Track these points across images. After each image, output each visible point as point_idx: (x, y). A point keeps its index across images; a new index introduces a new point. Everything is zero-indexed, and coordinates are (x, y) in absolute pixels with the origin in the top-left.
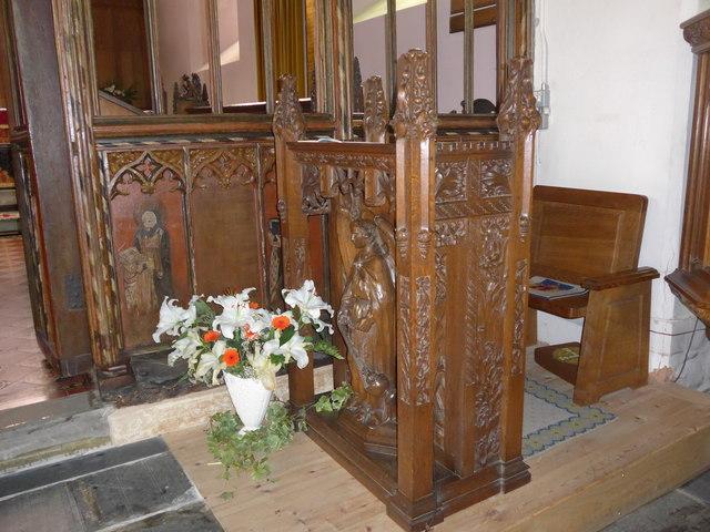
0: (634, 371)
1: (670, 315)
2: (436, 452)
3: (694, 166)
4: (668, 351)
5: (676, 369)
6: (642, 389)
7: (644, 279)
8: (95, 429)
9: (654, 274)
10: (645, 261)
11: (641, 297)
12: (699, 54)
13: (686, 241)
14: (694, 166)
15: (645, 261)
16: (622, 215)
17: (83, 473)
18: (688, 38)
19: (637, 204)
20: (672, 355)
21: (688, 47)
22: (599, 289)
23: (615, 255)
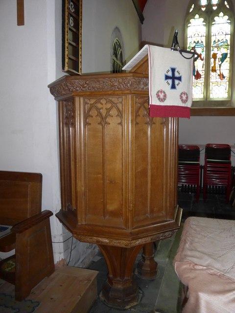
0: (49, 266)
1: (61, 232)
2: (178, 146)
3: (62, 154)
4: (62, 250)
5: (67, 258)
6: (52, 276)
7: (45, 218)
8: (19, 298)
9: (50, 213)
10: (45, 207)
11: (45, 227)
12: (59, 101)
13: (63, 196)
14: (62, 154)
15: (45, 207)
16: (30, 184)
17: (156, 226)
18: (52, 93)
19: (37, 178)
20: (64, 252)
21: (52, 97)
22: (21, 232)
23: (29, 206)
